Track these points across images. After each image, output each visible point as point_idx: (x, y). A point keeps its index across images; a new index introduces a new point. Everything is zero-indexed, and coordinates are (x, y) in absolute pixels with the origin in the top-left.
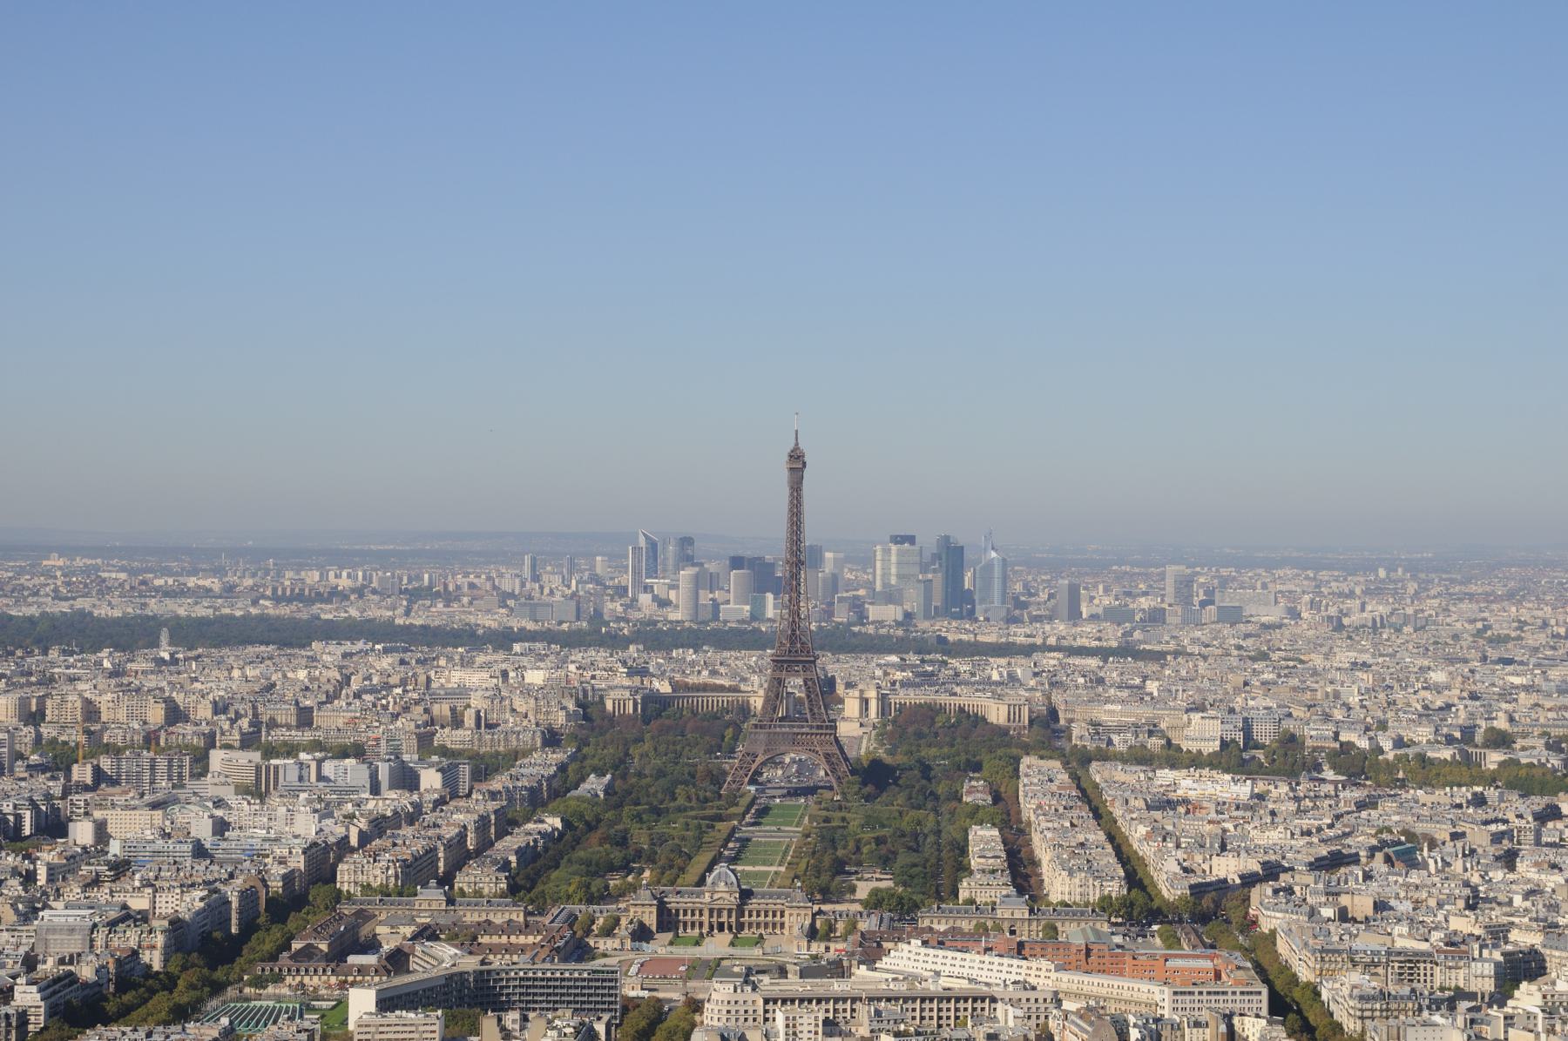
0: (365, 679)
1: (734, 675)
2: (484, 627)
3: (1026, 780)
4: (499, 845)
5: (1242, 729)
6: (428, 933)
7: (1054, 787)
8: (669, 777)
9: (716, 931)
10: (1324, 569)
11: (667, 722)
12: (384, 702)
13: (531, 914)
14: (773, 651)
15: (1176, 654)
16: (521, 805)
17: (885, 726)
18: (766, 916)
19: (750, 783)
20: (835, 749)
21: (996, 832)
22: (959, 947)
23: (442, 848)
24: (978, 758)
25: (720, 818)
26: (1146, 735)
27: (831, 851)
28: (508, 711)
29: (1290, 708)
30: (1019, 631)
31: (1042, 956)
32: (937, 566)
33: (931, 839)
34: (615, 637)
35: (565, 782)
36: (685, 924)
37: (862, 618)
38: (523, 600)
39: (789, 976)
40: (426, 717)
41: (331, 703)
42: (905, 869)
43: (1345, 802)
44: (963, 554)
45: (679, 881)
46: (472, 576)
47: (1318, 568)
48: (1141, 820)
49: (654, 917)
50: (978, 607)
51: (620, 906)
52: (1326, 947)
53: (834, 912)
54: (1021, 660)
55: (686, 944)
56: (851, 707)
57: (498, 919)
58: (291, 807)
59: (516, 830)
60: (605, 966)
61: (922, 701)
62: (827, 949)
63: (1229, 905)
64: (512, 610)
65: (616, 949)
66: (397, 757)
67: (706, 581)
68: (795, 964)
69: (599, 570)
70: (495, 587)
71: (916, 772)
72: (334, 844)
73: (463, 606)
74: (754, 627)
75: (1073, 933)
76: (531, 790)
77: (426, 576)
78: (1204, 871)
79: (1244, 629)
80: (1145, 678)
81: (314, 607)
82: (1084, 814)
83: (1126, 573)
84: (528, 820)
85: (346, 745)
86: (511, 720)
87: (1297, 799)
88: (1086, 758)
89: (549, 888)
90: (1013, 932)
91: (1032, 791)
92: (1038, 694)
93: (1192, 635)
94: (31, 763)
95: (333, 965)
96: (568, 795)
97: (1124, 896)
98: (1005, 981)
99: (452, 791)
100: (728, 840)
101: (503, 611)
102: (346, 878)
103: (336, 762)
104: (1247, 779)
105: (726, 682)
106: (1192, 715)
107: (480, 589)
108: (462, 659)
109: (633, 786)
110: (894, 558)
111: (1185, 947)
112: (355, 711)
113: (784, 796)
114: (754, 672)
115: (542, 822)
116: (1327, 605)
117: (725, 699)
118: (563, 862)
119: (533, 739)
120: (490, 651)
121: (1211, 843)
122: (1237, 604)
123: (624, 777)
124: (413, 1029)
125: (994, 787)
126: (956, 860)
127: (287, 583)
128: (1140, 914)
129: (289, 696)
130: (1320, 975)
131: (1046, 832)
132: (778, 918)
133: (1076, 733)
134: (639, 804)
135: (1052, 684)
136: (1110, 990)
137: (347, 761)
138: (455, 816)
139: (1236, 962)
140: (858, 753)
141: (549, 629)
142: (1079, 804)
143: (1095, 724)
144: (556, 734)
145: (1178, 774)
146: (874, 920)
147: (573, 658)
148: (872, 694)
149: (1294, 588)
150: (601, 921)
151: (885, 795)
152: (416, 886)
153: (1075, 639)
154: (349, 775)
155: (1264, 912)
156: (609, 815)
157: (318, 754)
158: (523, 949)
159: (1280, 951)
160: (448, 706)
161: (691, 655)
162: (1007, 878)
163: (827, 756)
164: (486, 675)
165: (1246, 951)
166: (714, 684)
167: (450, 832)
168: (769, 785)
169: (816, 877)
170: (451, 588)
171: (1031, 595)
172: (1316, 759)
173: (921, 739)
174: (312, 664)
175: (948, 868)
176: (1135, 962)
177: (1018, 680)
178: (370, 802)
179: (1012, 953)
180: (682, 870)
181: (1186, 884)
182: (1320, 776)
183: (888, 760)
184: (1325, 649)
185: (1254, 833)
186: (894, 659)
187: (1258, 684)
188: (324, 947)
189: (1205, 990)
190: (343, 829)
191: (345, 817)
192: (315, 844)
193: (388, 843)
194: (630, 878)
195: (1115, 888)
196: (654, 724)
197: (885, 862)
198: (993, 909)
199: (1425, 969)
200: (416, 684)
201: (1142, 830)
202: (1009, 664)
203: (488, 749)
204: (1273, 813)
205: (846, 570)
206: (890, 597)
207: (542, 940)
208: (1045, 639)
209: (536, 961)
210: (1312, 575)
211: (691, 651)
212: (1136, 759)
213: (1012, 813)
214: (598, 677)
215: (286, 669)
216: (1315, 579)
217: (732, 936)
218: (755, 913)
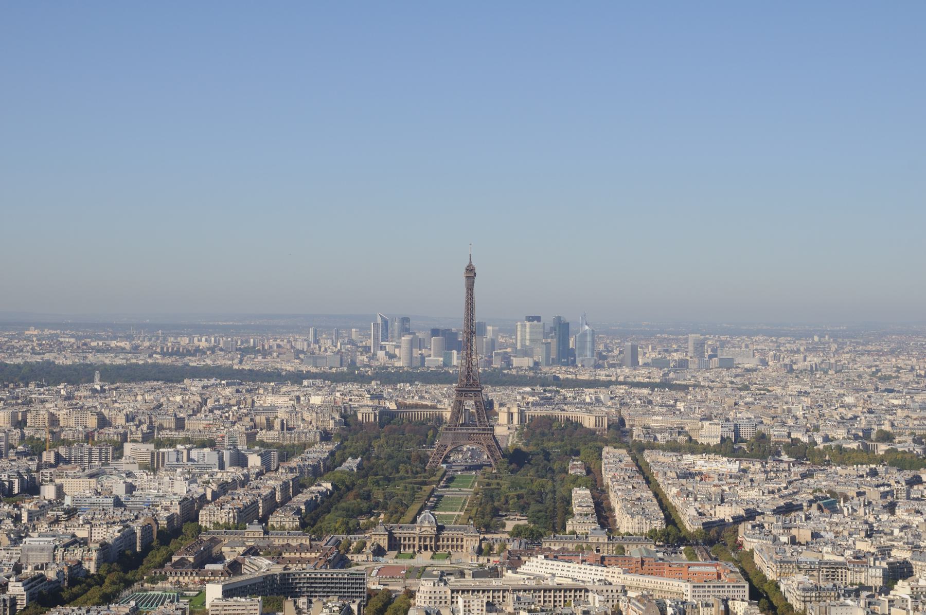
0: (215, 401)
1: (434, 399)
2: (286, 370)
3: (606, 461)
4: (295, 499)
5: (734, 431)
6: (253, 551)
7: (622, 465)
8: (395, 459)
9: (423, 550)
10: (782, 336)
11: (394, 426)
12: (227, 415)
13: (314, 540)
14: (456, 385)
15: (695, 386)
16: (308, 475)
17: (522, 429)
18: (452, 541)
19: (443, 463)
20: (493, 443)
21: (588, 492)
22: (567, 560)
23: (261, 501)
24: (578, 448)
25: (425, 483)
26: (677, 435)
27: (491, 503)
28: (300, 420)
29: (762, 418)
30: (602, 373)
31: (616, 565)
32: (553, 334)
33: (550, 496)
34: (363, 376)
35: (334, 462)
36: (405, 546)
37: (509, 365)
38: (309, 354)
39: (466, 576)
40: (251, 424)
41: (195, 415)
42: (534, 514)
43: (794, 474)
44: (569, 327)
45: (401, 520)
46: (279, 340)
47: (778, 335)
48: (674, 485)
49: (386, 542)
50: (577, 359)
51: (366, 535)
52: (783, 560)
53: (492, 539)
54: (603, 390)
55: (405, 558)
56: (503, 418)
57: (294, 543)
58: (172, 477)
59: (305, 491)
60: (357, 570)
61: (545, 414)
62: (489, 561)
63: (726, 534)
64: (302, 360)
65: (364, 561)
66: (235, 448)
67: (417, 343)
68: (470, 569)
69: (354, 337)
70: (292, 347)
71: (541, 456)
72: (197, 499)
73: (274, 358)
74: (445, 371)
75: (634, 551)
76: (314, 467)
77: (252, 340)
78: (711, 515)
79: (734, 371)
80: (676, 401)
81: (185, 359)
82: (640, 481)
83: (665, 338)
84: (312, 485)
85: (204, 440)
86: (302, 425)
87: (766, 472)
88: (641, 448)
89: (324, 524)
90: (598, 551)
91: (610, 467)
92: (613, 410)
93: (704, 375)
94: (18, 451)
95: (197, 570)
96: (336, 470)
97: (664, 529)
98: (593, 580)
99: (267, 467)
100: (430, 496)
101: (297, 361)
102: (204, 519)
103: (198, 450)
104: (736, 460)
105: (429, 403)
106: (704, 422)
107: (283, 348)
108: (273, 389)
109: (374, 464)
110: (528, 330)
111: (700, 559)
112: (210, 420)
113: (463, 470)
114: (445, 397)
115: (320, 485)
116: (784, 357)
117: (428, 413)
118: (333, 509)
119: (315, 436)
120: (289, 385)
121: (715, 498)
122: (731, 357)
123: (369, 459)
124: (244, 608)
125: (587, 465)
126: (564, 508)
127: (170, 344)
128: (673, 540)
129: (171, 411)
130: (780, 576)
131: (617, 491)
132: (459, 543)
133: (635, 433)
134: (377, 475)
135: (621, 404)
136: (655, 585)
137: (205, 449)
138: (268, 482)
139: (730, 568)
140: (507, 445)
141: (324, 372)
142: (637, 475)
143: (647, 428)
144: (329, 433)
145: (696, 457)
146: (516, 543)
147: (338, 389)
148: (515, 410)
149: (764, 348)
150: (355, 544)
151: (522, 469)
152: (246, 523)
153: (635, 378)
154: (206, 458)
155: (747, 539)
156: (360, 481)
157: (188, 446)
158: (309, 561)
159: (756, 562)
160: (264, 417)
161: (408, 387)
162: (595, 519)
163: (489, 447)
164: (287, 399)
165: (736, 562)
166: (422, 404)
167: (266, 492)
168: (454, 464)
169: (482, 518)
170: (266, 347)
171: (609, 351)
172: (777, 449)
173: (544, 436)
174: (184, 392)
175: (560, 513)
176: (670, 568)
177: (601, 402)
178: (219, 474)
179: (597, 563)
180: (403, 514)
181: (700, 522)
182: (780, 459)
183: (524, 449)
184: (782, 384)
185: (740, 492)
186: (528, 389)
187: (743, 404)
188: (191, 559)
189: (711, 585)
190: (203, 490)
191: (204, 483)
192: (186, 499)
193: (229, 498)
194: (372, 519)
195: (659, 524)
196: (386, 428)
197: (523, 509)
198: (586, 537)
199: (842, 572)
200: (246, 404)
201: (675, 490)
202: (596, 392)
203: (288, 442)
204: (752, 481)
205: (500, 337)
206: (526, 353)
207: (320, 556)
208: (617, 378)
209: (317, 568)
210: (775, 340)
211: (408, 385)
212: (671, 448)
213: (598, 480)
214: (353, 400)
215: (169, 395)
216: (776, 342)
217: (432, 553)
218: (446, 540)
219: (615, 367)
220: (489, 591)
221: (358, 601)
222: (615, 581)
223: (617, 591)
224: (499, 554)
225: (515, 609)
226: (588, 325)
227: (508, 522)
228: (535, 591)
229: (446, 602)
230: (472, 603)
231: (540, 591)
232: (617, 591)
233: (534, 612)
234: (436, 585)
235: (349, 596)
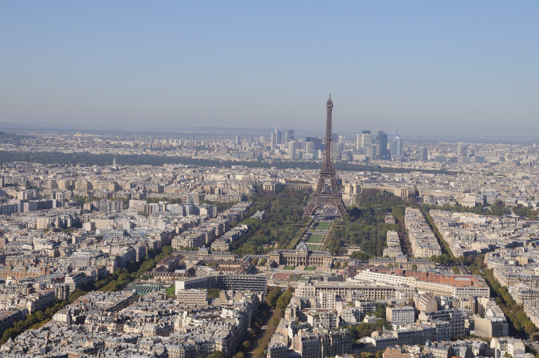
0: (181, 177)
3: (407, 216)
4: (226, 234)
6: (202, 263)
7: (417, 218)
12: (188, 185)
13: (237, 257)
15: (461, 173)
16: (234, 220)
17: (359, 196)
18: (317, 260)
19: (312, 215)
21: (396, 233)
25: (301, 227)
35: (249, 213)
36: (289, 262)
37: (351, 159)
38: (235, 151)
40: (202, 190)
45: (287, 247)
47: (511, 144)
48: (447, 230)
50: (392, 156)
51: (267, 255)
52: (511, 274)
54: (406, 174)
55: (289, 269)
56: (347, 189)
57: (226, 259)
59: (232, 229)
62: (337, 272)
64: (231, 154)
67: (298, 145)
69: (261, 141)
70: (226, 146)
75: (422, 268)
76: (237, 216)
77: (202, 142)
78: (468, 248)
80: (449, 181)
82: (427, 227)
83: (444, 144)
84: (236, 226)
86: (231, 192)
87: (502, 224)
88: (428, 208)
89: (243, 249)
90: (401, 267)
92: (412, 186)
93: (466, 166)
95: (170, 273)
100: (304, 234)
102: (175, 244)
103: (171, 205)
105: (304, 180)
107: (221, 147)
108: (214, 171)
110: (363, 139)
111: (461, 273)
114: (314, 177)
115: (241, 226)
118: (248, 240)
119: (238, 198)
120: (224, 168)
123: (269, 212)
125: (396, 218)
126: (382, 242)
127: (156, 144)
128: (446, 262)
129: (156, 182)
132: (321, 261)
133: (425, 199)
135: (417, 183)
136: (435, 288)
137: (175, 204)
138: (211, 224)
139: (479, 279)
140: (349, 205)
142: (426, 224)
143: (432, 197)
144: (246, 197)
146: (354, 262)
147: (252, 171)
148: (354, 185)
153: (425, 167)
156: (264, 225)
157: (165, 202)
158: (234, 269)
161: (292, 171)
162: (400, 249)
163: (339, 206)
164: (222, 176)
165: (482, 275)
167: (210, 229)
170: (211, 146)
171: (410, 152)
172: (509, 210)
175: (379, 245)
176: (444, 278)
177: (405, 181)
180: (288, 244)
181: (462, 252)
183: (359, 208)
184: (513, 172)
185: (486, 235)
186: (362, 173)
187: (489, 183)
188: (167, 267)
189: (468, 288)
191: (174, 223)
192: (164, 232)
193: (189, 233)
194: (270, 246)
195: (437, 253)
196: (279, 194)
197: (358, 242)
198: (395, 259)
201: (447, 233)
202: (402, 175)
204: (493, 228)
206: (361, 152)
207: (240, 266)
208: (415, 167)
211: (292, 169)
216: (510, 147)
218: (313, 259)
220: (337, 289)
221: (262, 293)
223: (412, 290)
225: (352, 300)
226: (398, 136)
227: (349, 250)
228: (364, 289)
229: (312, 295)
230: (328, 296)
231: (367, 289)
232: (412, 290)
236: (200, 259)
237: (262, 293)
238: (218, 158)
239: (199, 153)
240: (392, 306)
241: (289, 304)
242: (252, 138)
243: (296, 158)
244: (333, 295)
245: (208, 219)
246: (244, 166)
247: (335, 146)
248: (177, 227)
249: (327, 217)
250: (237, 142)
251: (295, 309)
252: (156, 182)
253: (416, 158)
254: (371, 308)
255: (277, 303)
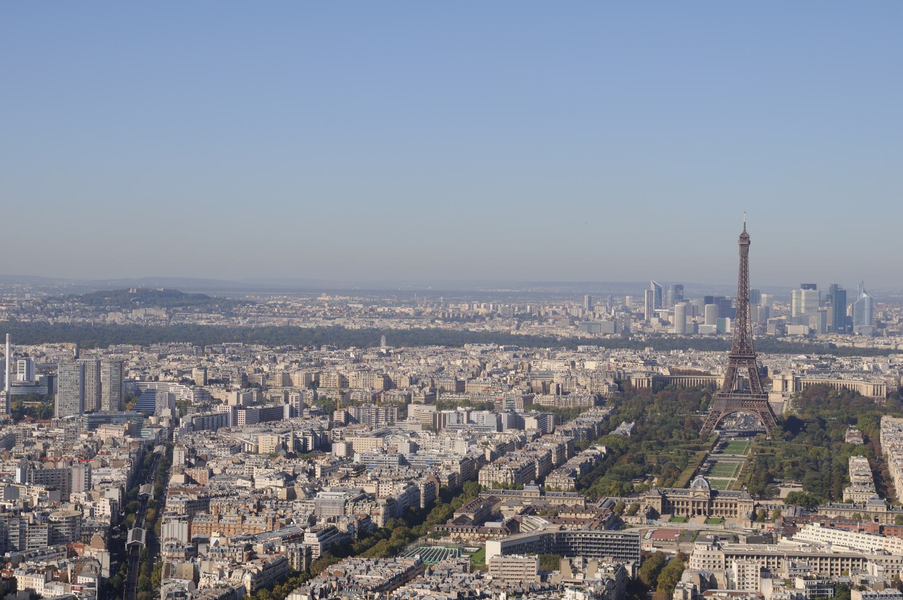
0: (494, 366)
2: (561, 336)
3: (884, 430)
4: (570, 462)
6: (530, 511)
8: (668, 425)
9: (696, 514)
11: (667, 392)
12: (505, 378)
13: (589, 501)
14: (730, 352)
16: (583, 438)
17: (797, 396)
18: (726, 506)
19: (716, 429)
20: (767, 410)
21: (866, 461)
22: (843, 528)
23: (538, 463)
25: (699, 449)
27: (765, 469)
30: (880, 341)
31: (895, 535)
32: (830, 302)
35: (608, 426)
36: (678, 510)
37: (784, 332)
38: (583, 321)
40: (528, 387)
45: (675, 485)
46: (554, 307)
49: (660, 505)
50: (855, 327)
51: (640, 498)
53: (767, 505)
54: (881, 358)
55: (678, 521)
56: (777, 385)
57: (570, 504)
59: (580, 453)
60: (631, 532)
61: (820, 382)
62: (763, 527)
64: (577, 327)
65: (638, 523)
66: (512, 410)
68: (744, 535)
69: (627, 304)
70: (567, 314)
71: (817, 424)
72: (477, 459)
76: (588, 430)
77: (528, 307)
81: (466, 324)
84: (587, 448)
86: (577, 390)
89: (599, 487)
90: (877, 520)
91: (889, 436)
92: (892, 379)
95: (477, 527)
98: (872, 549)
99: (543, 430)
100: (703, 461)
103: (477, 412)
105: (702, 370)
108: (549, 354)
110: (803, 298)
112: (489, 384)
113: (737, 436)
114: (719, 364)
115: (595, 449)
117: (701, 379)
118: (607, 473)
119: (589, 401)
120: (565, 350)
123: (642, 423)
125: (865, 434)
126: (841, 477)
127: (451, 311)
129: (452, 374)
131: (897, 461)
132: (733, 508)
134: (651, 440)
138: (545, 445)
144: (603, 398)
147: (612, 355)
148: (789, 377)
150: (629, 507)
154: (485, 420)
156: (633, 446)
158: (584, 521)
161: (681, 354)
162: (873, 488)
163: (763, 414)
164: (562, 364)
166: (695, 370)
167: (542, 454)
168: (728, 430)
170: (542, 314)
171: (888, 320)
174: (464, 357)
177: (880, 370)
178: (497, 435)
180: (676, 478)
186: (803, 357)
188: (471, 517)
190: (482, 451)
191: (483, 444)
192: (466, 459)
193: (507, 459)
194: (646, 483)
196: (660, 394)
197: (798, 477)
198: (864, 506)
200: (523, 369)
202: (874, 360)
203: (564, 406)
205: (774, 304)
206: (801, 320)
207: (595, 517)
209: (592, 529)
211: (681, 351)
213: (876, 449)
217: (706, 517)
218: (719, 505)
219: (894, 335)
220: (763, 557)
221: (632, 562)
222: (894, 551)
223: (897, 561)
224: (773, 521)
225: (790, 576)
226: (866, 293)
228: (811, 558)
229: (720, 567)
230: (747, 568)
231: (816, 558)
232: (897, 561)
233: (809, 579)
234: (710, 549)
235: (624, 557)
236: (527, 503)
237: (632, 562)
238: (555, 333)
239: (522, 324)
240: (861, 589)
241: (680, 582)
242: (611, 299)
243: (687, 333)
244: (757, 567)
245: (540, 437)
246: (599, 346)
247: (755, 311)
248: (487, 450)
249: (744, 433)
250: (586, 305)
251: (689, 591)
252: (452, 374)
253: (898, 330)
254: (823, 591)
255: (659, 581)
